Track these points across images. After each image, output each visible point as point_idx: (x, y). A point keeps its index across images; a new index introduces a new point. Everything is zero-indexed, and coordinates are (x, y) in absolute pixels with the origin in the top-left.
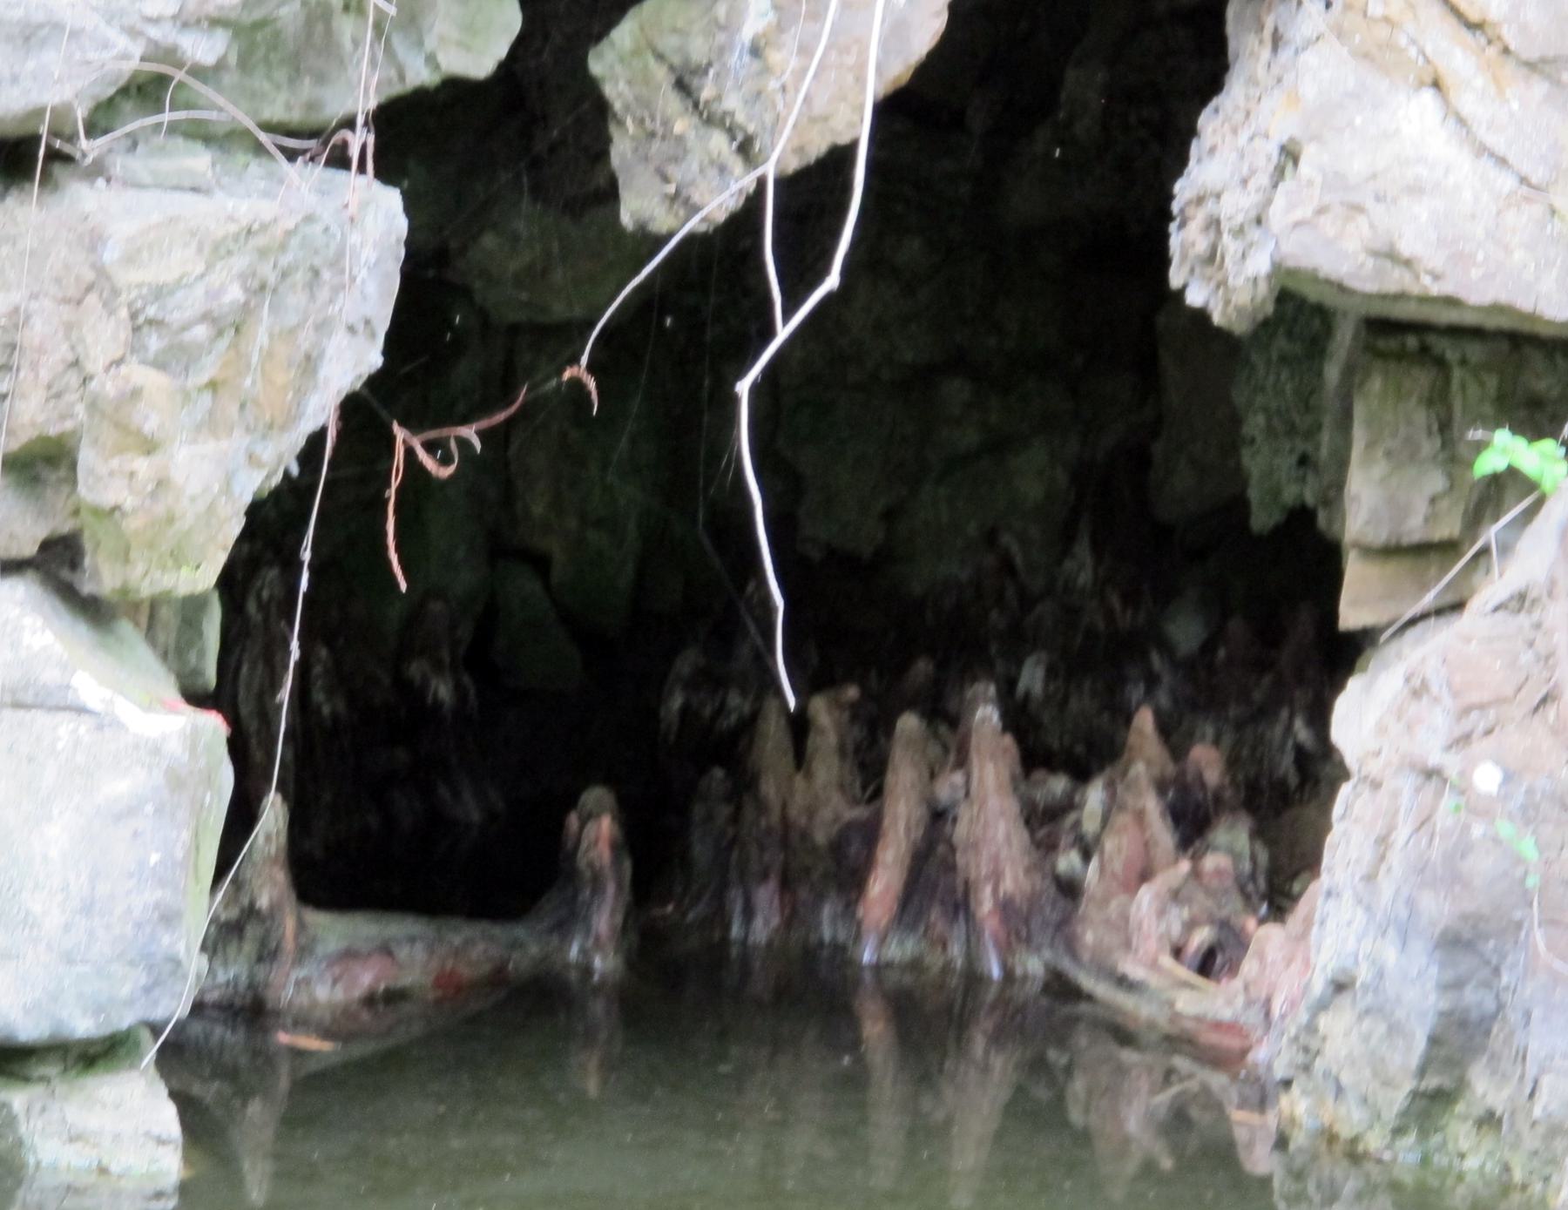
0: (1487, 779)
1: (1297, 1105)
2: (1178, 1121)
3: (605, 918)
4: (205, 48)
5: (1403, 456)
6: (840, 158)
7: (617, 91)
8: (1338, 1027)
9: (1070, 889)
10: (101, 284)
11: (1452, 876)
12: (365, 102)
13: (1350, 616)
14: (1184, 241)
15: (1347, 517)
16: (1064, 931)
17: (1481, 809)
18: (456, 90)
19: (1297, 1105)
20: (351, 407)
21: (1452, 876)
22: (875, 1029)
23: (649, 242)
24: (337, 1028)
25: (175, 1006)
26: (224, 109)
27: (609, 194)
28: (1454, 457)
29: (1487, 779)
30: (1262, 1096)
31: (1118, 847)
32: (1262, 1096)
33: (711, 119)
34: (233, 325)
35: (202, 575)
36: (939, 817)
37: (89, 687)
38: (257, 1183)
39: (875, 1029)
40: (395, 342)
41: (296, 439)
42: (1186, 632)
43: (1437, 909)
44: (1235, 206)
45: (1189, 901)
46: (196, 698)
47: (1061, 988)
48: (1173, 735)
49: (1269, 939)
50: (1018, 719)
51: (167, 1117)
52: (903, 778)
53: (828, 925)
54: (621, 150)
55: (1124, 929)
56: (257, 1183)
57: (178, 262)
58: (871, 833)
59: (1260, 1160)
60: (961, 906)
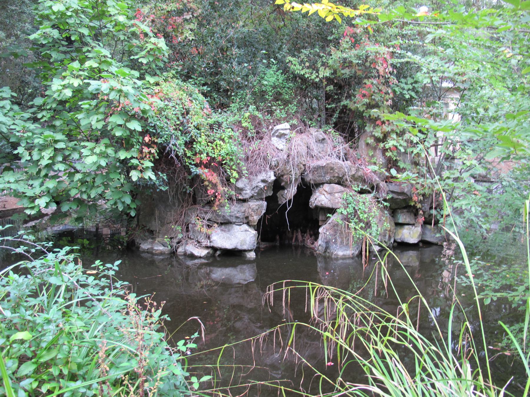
0: (328, 233)
1: (318, 252)
2: (310, 253)
3: (278, 242)
4: (255, 194)
5: (322, 215)
6: (291, 200)
7: (278, 196)
8: (320, 248)
9: (304, 240)
10: (250, 207)
11: (326, 239)
12: (264, 197)
13: (320, 224)
14: (310, 204)
15: (408, 242)
16: (304, 242)
17: (327, 235)
18: (269, 196)
19: (318, 252)
20: (264, 214)
21: (326, 239)
22: (293, 248)
23: (280, 205)
24: (263, 248)
25: (255, 248)
26: (256, 198)
27: (278, 202)
28: (326, 215)
29: (328, 233)
30: (316, 251)
31: (307, 237)
32: (316, 251)
33: (284, 197)
34: (257, 210)
35: (256, 224)
36: (297, 236)
37: (250, 230)
38: (259, 257)
39: (293, 248)
40: (266, 210)
41: (260, 216)
42: (310, 225)
43: (325, 241)
44: (313, 202)
45: (438, 39)
46: (256, 230)
47: (304, 245)
48: (310, 231)
49: (316, 242)
50: (301, 230)
51: (255, 254)
52: (295, 234)
53: (291, 242)
54: (279, 199)
55: (307, 242)
56: (259, 257)
57: (254, 206)
58: (293, 237)
59: (315, 255)
60: (298, 241)
